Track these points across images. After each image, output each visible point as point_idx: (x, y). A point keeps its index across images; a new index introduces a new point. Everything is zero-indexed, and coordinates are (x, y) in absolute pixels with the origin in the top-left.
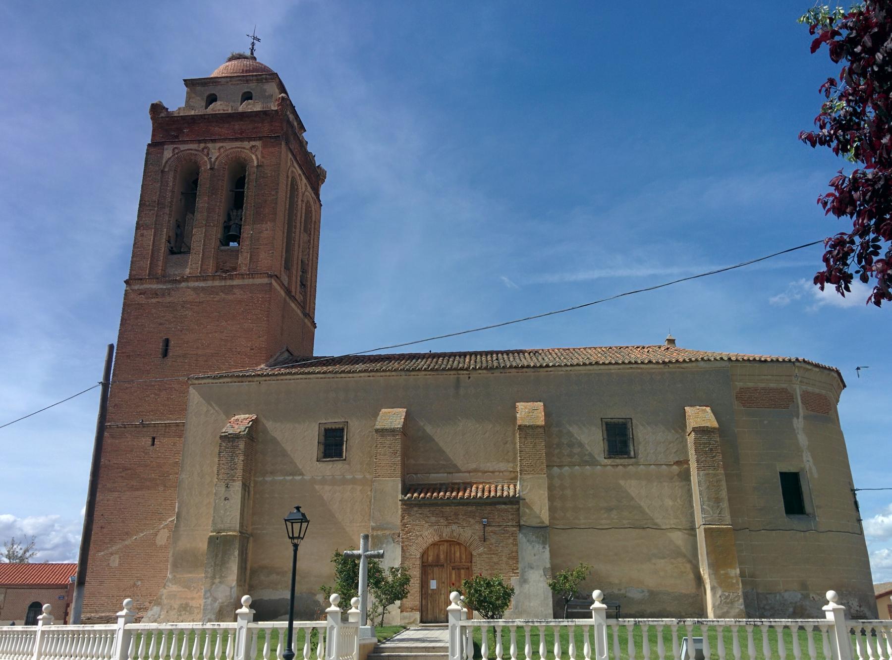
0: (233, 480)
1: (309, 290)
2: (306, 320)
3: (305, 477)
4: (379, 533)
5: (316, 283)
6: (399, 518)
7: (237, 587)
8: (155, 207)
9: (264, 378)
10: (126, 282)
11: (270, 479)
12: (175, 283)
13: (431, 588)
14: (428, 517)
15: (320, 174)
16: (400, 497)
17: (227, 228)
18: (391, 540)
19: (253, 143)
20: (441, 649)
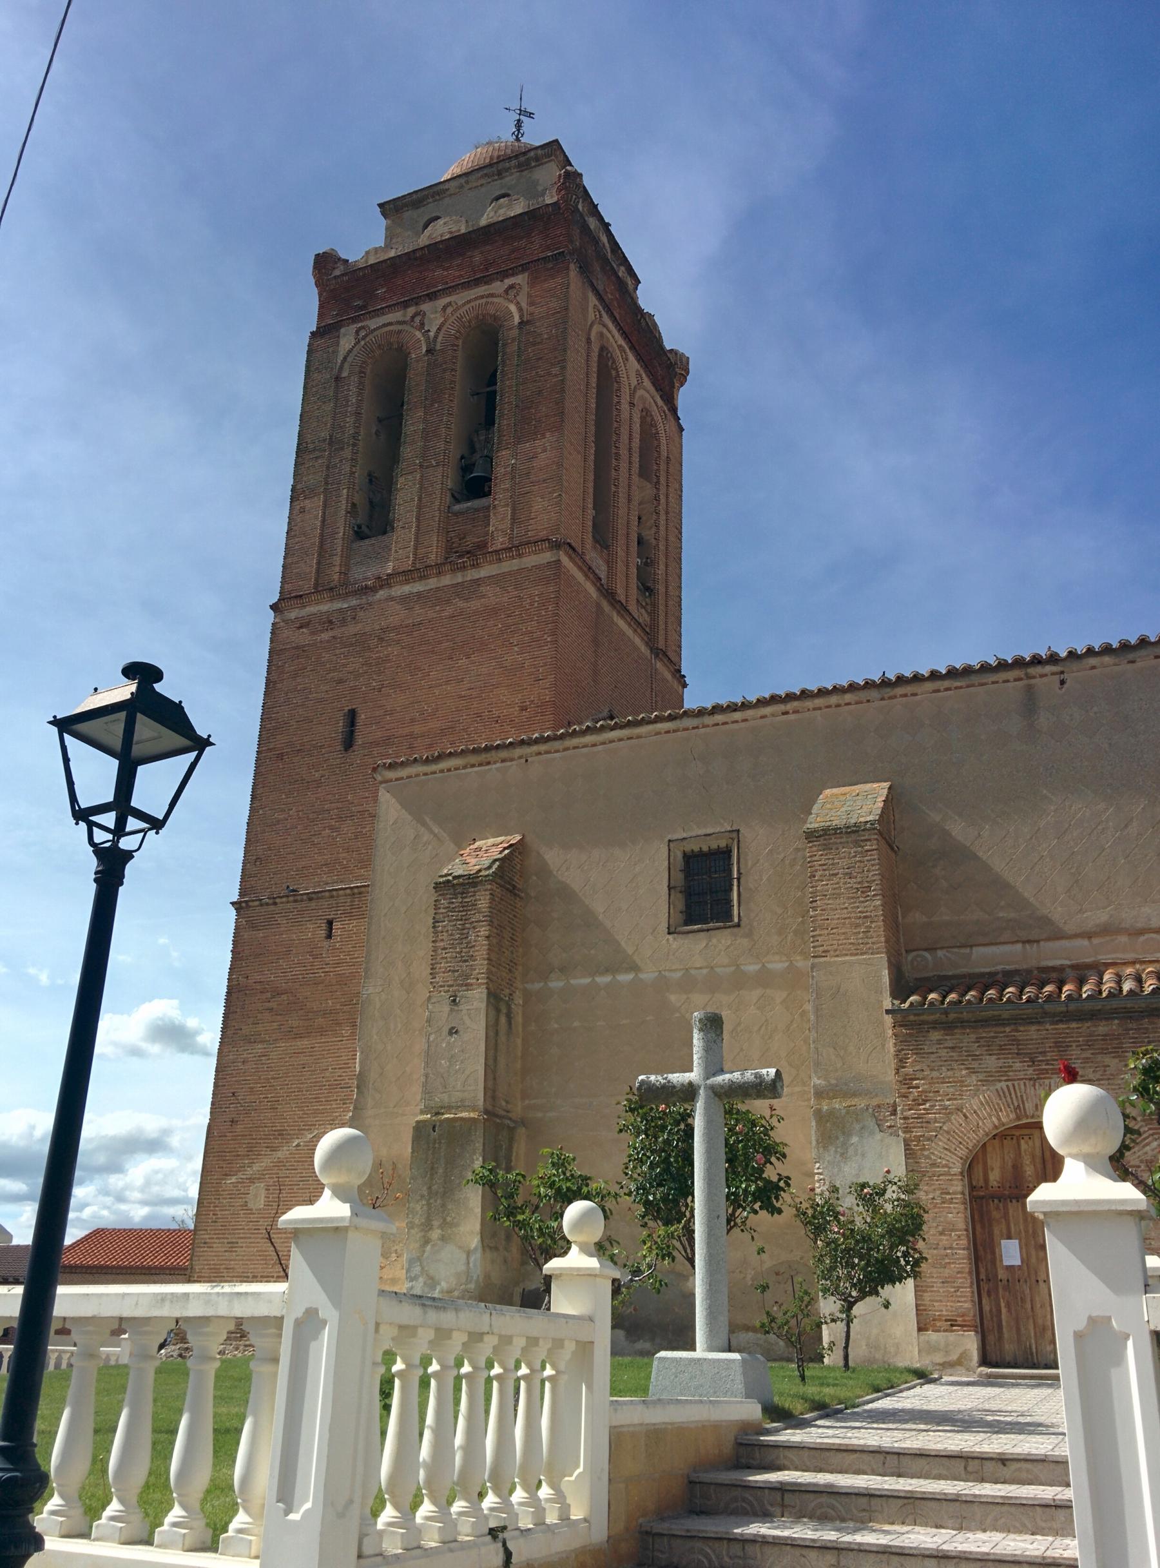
0: (466, 985)
1: (661, 601)
2: (659, 665)
3: (642, 976)
4: (837, 1104)
5: (681, 592)
6: (893, 1063)
7: (484, 1250)
8: (325, 451)
9: (535, 748)
10: (274, 607)
11: (561, 984)
12: (365, 594)
13: (1006, 1263)
14: (976, 1058)
15: (676, 364)
16: (887, 1003)
17: (466, 468)
18: (871, 1123)
19: (509, 281)
20: (1036, 1469)
